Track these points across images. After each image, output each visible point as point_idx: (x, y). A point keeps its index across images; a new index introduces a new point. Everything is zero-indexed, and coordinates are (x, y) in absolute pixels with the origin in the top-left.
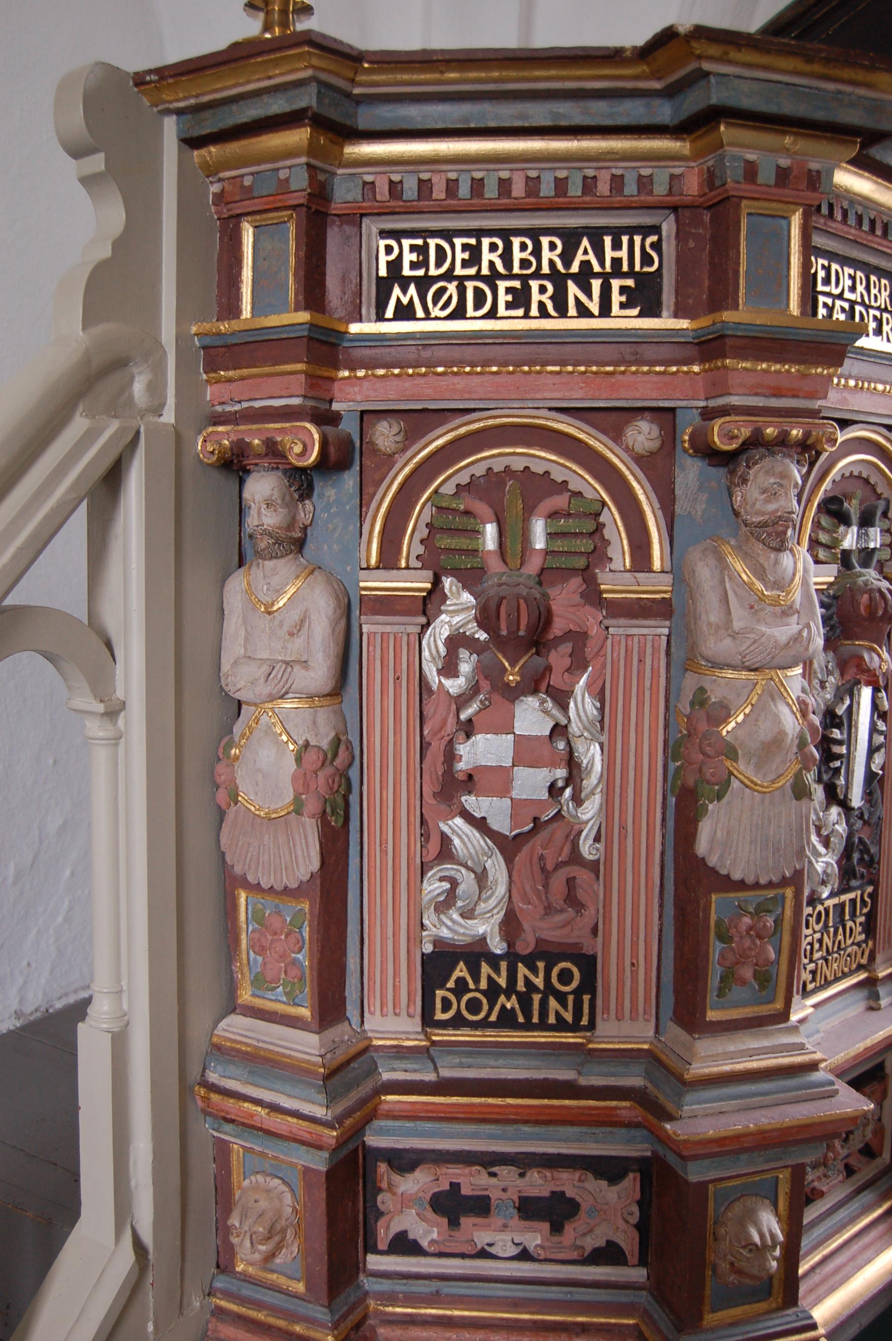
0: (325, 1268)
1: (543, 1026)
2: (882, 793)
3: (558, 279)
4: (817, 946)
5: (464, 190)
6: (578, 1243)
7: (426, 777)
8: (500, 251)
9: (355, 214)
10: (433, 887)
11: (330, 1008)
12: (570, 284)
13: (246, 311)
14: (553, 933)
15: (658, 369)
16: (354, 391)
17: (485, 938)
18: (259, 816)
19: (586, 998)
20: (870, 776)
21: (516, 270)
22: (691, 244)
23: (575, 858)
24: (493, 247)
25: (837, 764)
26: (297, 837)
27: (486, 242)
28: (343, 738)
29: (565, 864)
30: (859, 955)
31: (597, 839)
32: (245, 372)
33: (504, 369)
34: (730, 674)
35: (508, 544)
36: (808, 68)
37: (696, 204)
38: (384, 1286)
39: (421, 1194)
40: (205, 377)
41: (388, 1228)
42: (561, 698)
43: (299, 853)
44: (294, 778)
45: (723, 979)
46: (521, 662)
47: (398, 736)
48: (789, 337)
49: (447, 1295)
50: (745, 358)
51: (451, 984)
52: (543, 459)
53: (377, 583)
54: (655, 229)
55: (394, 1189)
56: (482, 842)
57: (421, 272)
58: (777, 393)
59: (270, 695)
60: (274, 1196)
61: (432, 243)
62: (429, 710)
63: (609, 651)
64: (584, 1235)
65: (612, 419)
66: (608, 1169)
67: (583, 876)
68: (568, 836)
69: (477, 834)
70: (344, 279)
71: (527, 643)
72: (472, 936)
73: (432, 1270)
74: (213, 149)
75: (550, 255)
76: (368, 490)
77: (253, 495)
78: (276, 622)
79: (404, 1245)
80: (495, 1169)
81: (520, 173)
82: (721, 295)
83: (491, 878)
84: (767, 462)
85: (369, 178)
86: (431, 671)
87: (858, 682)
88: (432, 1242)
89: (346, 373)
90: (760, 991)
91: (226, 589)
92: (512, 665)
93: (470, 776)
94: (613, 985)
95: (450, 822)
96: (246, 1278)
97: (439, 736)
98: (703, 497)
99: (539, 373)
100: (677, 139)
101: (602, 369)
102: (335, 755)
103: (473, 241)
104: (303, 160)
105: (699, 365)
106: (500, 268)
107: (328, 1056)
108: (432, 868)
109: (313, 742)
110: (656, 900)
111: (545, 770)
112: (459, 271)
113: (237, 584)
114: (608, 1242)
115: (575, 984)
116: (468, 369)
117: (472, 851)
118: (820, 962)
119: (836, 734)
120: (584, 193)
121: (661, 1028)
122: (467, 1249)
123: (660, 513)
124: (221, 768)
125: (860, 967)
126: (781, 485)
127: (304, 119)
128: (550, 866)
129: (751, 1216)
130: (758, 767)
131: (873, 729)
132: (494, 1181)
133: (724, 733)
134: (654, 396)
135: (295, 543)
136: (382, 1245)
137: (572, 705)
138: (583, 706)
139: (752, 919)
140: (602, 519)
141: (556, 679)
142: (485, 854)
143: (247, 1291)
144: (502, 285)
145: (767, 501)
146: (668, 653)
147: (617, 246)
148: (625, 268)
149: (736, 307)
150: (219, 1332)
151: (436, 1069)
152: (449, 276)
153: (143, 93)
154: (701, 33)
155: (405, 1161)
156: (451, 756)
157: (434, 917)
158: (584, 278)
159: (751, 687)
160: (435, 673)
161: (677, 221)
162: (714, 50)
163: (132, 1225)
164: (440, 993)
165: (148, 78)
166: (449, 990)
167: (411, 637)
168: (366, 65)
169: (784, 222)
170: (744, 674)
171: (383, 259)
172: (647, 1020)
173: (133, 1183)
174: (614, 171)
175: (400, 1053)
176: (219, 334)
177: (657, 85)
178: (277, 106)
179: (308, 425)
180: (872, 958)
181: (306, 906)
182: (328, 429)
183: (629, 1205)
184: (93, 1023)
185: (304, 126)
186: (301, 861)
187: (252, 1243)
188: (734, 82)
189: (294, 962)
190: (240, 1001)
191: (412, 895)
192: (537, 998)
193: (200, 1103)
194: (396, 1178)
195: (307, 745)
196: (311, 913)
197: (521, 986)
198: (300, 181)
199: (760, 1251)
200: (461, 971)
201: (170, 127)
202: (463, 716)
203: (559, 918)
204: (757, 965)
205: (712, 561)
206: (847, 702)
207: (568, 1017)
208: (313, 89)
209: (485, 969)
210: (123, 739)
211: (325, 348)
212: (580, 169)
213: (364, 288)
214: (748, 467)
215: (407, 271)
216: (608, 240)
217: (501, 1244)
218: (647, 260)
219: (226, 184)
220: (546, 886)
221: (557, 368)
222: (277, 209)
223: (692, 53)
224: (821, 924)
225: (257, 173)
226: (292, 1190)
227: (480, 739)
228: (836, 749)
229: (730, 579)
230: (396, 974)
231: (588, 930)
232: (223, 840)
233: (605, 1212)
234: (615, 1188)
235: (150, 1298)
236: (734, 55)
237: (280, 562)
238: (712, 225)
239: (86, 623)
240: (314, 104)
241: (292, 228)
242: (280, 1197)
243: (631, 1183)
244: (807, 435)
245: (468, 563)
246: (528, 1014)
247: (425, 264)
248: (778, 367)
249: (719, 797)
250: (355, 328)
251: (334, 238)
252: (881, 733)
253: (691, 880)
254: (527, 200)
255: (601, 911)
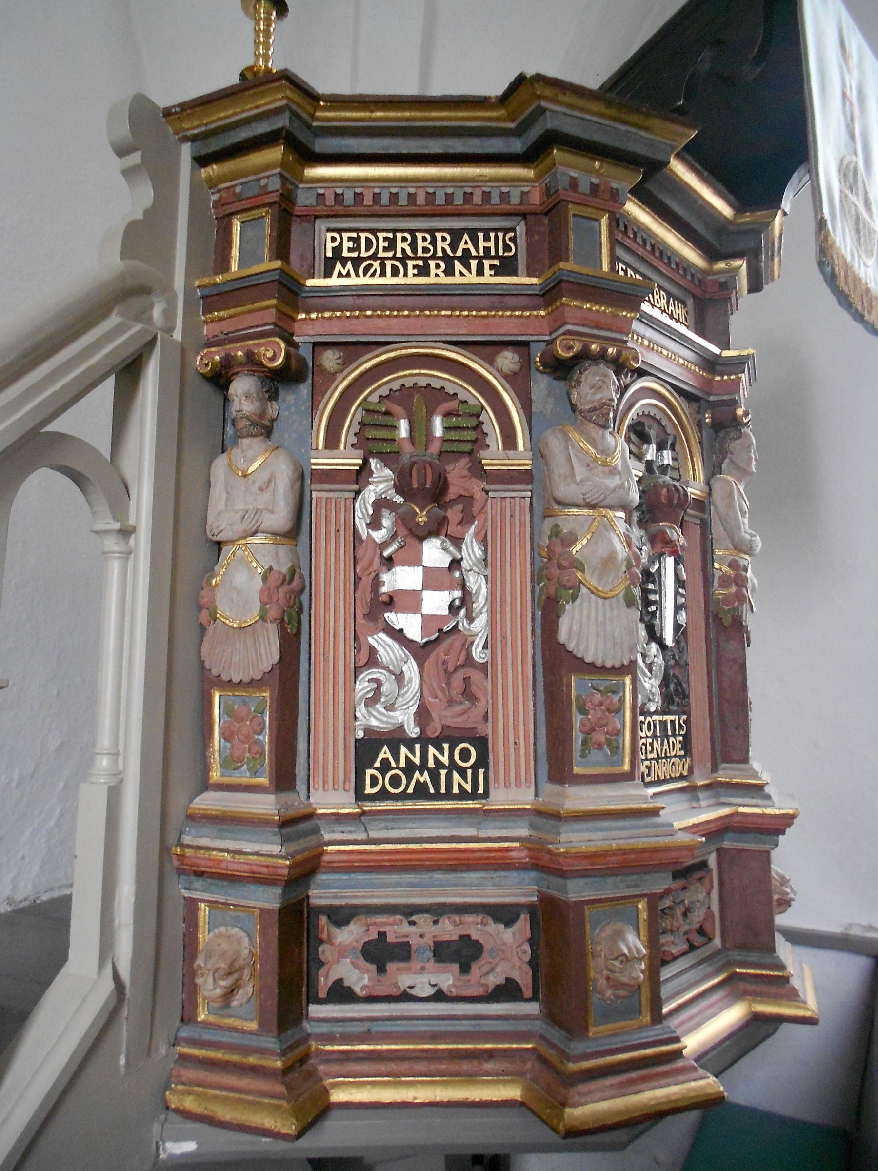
0: (276, 1001)
1: (449, 796)
2: (686, 642)
3: (448, 260)
4: (649, 748)
5: (385, 200)
6: (483, 981)
7: (358, 603)
8: (409, 242)
9: (310, 215)
10: (363, 687)
11: (284, 778)
12: (456, 261)
13: (234, 266)
14: (454, 720)
15: (517, 313)
16: (310, 329)
17: (403, 726)
18: (232, 627)
19: (481, 771)
20: (677, 626)
21: (420, 254)
22: (536, 237)
23: (469, 661)
24: (404, 239)
25: (653, 608)
26: (262, 640)
27: (399, 236)
28: (298, 571)
29: (462, 666)
30: (681, 767)
31: (485, 647)
32: (232, 311)
33: (413, 314)
34: (575, 511)
35: (417, 434)
36: (608, 112)
37: (538, 211)
38: (324, 1028)
39: (354, 944)
40: (203, 318)
41: (327, 976)
42: (458, 542)
43: (263, 652)
44: (261, 593)
45: (584, 742)
46: (428, 509)
47: (337, 573)
48: (605, 287)
49: (377, 1033)
50: (575, 298)
51: (377, 764)
52: (440, 378)
53: (322, 461)
54: (513, 230)
55: (333, 940)
56: (401, 653)
57: (355, 254)
58: (598, 327)
59: (245, 531)
60: (232, 936)
61: (363, 236)
62: (360, 552)
63: (489, 512)
64: (488, 973)
65: (486, 348)
66: (504, 914)
67: (476, 676)
68: (464, 645)
69: (397, 646)
70: (302, 258)
71: (431, 500)
72: (394, 724)
73: (363, 1015)
74: (215, 167)
75: (443, 245)
76: (316, 398)
77: (236, 390)
78: (250, 482)
79: (341, 993)
80: (414, 918)
81: (422, 189)
82: (558, 253)
83: (407, 679)
84: (593, 368)
85: (321, 191)
86: (361, 526)
87: (663, 554)
88: (364, 987)
89: (304, 316)
90: (612, 756)
91: (213, 465)
92: (421, 510)
93: (391, 598)
94: (502, 759)
95: (375, 637)
96: (206, 1024)
97: (367, 572)
98: (551, 400)
99: (436, 316)
100: (525, 167)
101: (479, 314)
102: (292, 579)
103: (390, 235)
104: (278, 170)
105: (545, 310)
106: (409, 252)
107: (283, 810)
108: (362, 673)
109: (275, 568)
110: (531, 691)
111: (447, 593)
112: (381, 254)
113: (220, 464)
114: (507, 979)
115: (473, 760)
116: (388, 313)
117: (392, 657)
118: (653, 762)
119: (651, 586)
120: (464, 203)
121: (540, 792)
122: (394, 992)
123: (521, 411)
124: (203, 593)
125: (682, 778)
126: (604, 382)
127: (278, 139)
128: (451, 668)
129: (619, 935)
130: (600, 578)
131: (677, 593)
132: (413, 929)
133: (574, 551)
134: (515, 332)
135: (265, 429)
136: (322, 994)
137: (464, 547)
138: (471, 551)
139: (602, 696)
140: (481, 418)
141: (452, 529)
142: (402, 659)
143: (207, 1036)
144: (410, 263)
145: (594, 393)
146: (531, 510)
147: (487, 239)
148: (493, 253)
149: (567, 260)
150: (181, 1076)
151: (366, 831)
152: (374, 257)
153: (169, 123)
154: (539, 78)
155: (341, 916)
156: (377, 583)
157: (364, 710)
158: (465, 259)
159: (590, 521)
160: (365, 527)
161: (526, 224)
162: (548, 92)
163: (113, 963)
164: (369, 772)
165: (173, 110)
166: (376, 769)
167: (348, 501)
168: (322, 103)
169: (596, 224)
170: (585, 511)
171: (330, 245)
172: (528, 787)
173: (116, 922)
174: (484, 189)
175: (338, 818)
176: (215, 285)
177: (512, 125)
178: (262, 128)
179: (277, 339)
180: (691, 771)
181: (267, 694)
182: (291, 349)
183: (522, 943)
184: (94, 780)
185: (279, 145)
186: (264, 657)
187: (214, 980)
188: (561, 117)
189: (257, 742)
190: (211, 781)
191: (348, 693)
192: (443, 772)
193: (176, 863)
194: (335, 930)
195: (271, 569)
196: (271, 698)
197: (431, 764)
198: (275, 184)
199: (627, 960)
200: (385, 753)
201: (186, 151)
202: (386, 554)
203: (458, 709)
204: (607, 733)
205: (560, 435)
206: (657, 565)
207: (468, 787)
208: (287, 115)
209: (404, 751)
210: (132, 556)
211: (289, 291)
212: (462, 187)
213: (316, 265)
214: (581, 373)
215: (345, 254)
216: (481, 235)
217: (420, 986)
218: (507, 248)
219: (223, 194)
220: (448, 684)
221: (449, 313)
222: (258, 207)
223: (535, 93)
224: (651, 732)
225: (245, 183)
226: (249, 935)
227: (398, 569)
228: (652, 597)
229: (572, 447)
230: (335, 756)
231: (480, 718)
232: (204, 651)
233: (503, 951)
234: (511, 930)
235: (124, 1031)
236: (561, 97)
237: (255, 440)
238: (549, 223)
239: (109, 459)
240: (287, 124)
241: (268, 220)
242: (239, 941)
243: (523, 923)
244: (619, 354)
245: (387, 448)
246: (437, 786)
247: (358, 249)
248: (597, 307)
249: (574, 598)
250: (310, 283)
251: (296, 229)
252: (683, 596)
253: (556, 663)
254: (427, 208)
255: (490, 701)
